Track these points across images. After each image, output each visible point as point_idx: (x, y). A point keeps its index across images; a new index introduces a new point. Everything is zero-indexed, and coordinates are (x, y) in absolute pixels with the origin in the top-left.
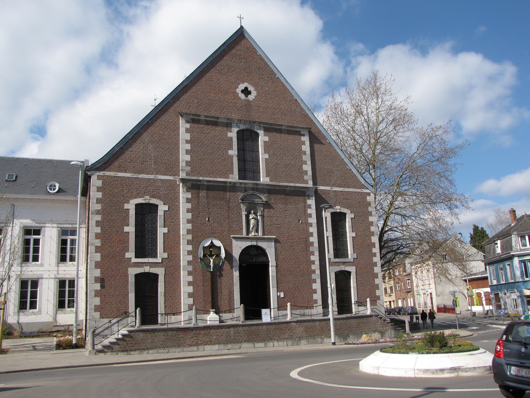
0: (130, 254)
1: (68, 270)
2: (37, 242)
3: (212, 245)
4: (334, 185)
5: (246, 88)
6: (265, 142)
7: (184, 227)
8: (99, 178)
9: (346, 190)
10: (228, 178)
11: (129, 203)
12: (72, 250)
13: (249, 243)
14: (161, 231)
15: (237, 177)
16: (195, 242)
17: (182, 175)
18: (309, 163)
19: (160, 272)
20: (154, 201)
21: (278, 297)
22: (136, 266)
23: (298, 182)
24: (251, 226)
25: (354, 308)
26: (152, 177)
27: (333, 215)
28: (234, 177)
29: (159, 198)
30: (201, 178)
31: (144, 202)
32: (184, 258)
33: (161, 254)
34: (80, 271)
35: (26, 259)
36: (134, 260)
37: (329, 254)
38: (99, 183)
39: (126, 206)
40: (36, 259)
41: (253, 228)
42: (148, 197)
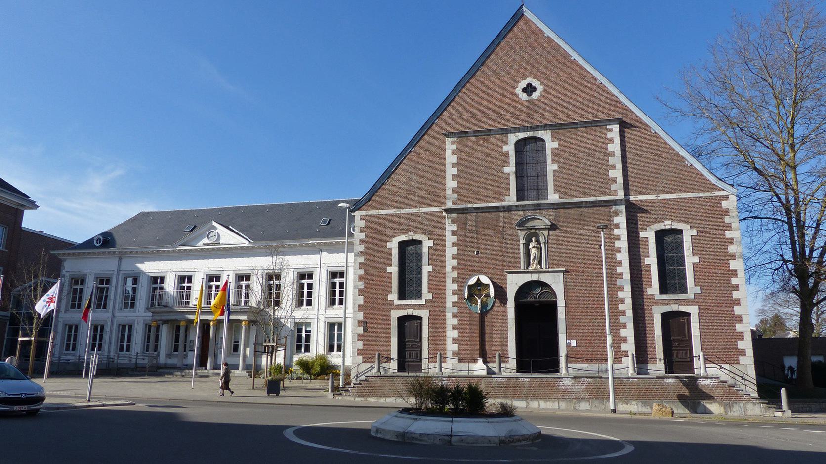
0: (393, 296)
1: (336, 313)
2: (310, 286)
3: (479, 283)
4: (662, 192)
5: (529, 85)
6: (553, 149)
7: (450, 263)
8: (362, 218)
9: (683, 195)
10: (503, 201)
11: (391, 241)
12: (341, 293)
13: (527, 278)
14: (427, 269)
15: (515, 198)
16: (460, 280)
17: (449, 205)
18: (619, 166)
19: (424, 314)
20: (417, 237)
21: (568, 345)
22: (399, 308)
23: (602, 195)
24: (532, 257)
25: (425, 363)
26: (415, 210)
27: (660, 235)
28: (511, 199)
29: (684, 222)
30: (470, 206)
31: (407, 239)
32: (451, 299)
33: (427, 295)
34: (349, 313)
35: (300, 304)
36: (398, 302)
37: (653, 288)
38: (362, 223)
39: (389, 245)
40: (309, 303)
41: (534, 259)
42: (411, 234)
